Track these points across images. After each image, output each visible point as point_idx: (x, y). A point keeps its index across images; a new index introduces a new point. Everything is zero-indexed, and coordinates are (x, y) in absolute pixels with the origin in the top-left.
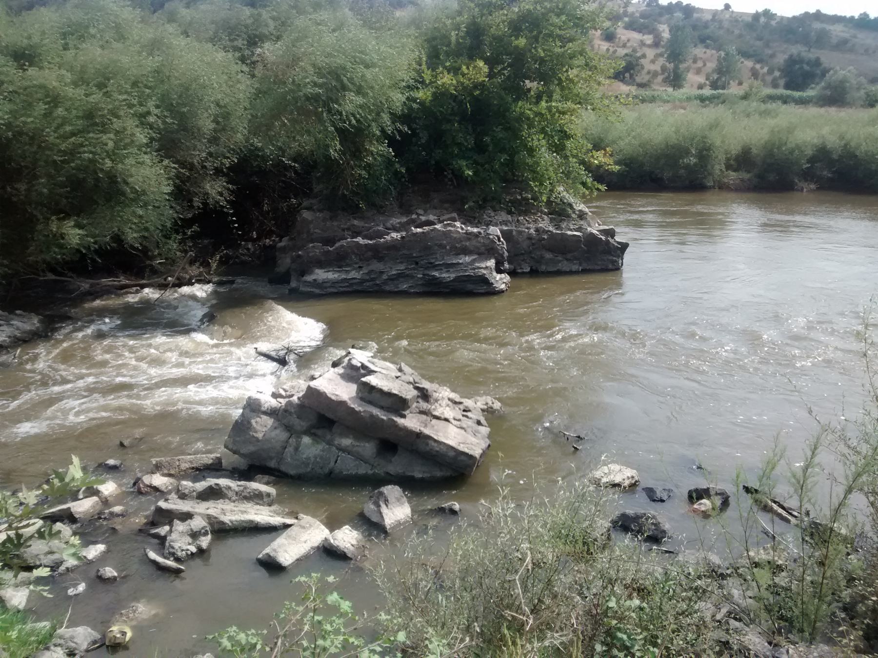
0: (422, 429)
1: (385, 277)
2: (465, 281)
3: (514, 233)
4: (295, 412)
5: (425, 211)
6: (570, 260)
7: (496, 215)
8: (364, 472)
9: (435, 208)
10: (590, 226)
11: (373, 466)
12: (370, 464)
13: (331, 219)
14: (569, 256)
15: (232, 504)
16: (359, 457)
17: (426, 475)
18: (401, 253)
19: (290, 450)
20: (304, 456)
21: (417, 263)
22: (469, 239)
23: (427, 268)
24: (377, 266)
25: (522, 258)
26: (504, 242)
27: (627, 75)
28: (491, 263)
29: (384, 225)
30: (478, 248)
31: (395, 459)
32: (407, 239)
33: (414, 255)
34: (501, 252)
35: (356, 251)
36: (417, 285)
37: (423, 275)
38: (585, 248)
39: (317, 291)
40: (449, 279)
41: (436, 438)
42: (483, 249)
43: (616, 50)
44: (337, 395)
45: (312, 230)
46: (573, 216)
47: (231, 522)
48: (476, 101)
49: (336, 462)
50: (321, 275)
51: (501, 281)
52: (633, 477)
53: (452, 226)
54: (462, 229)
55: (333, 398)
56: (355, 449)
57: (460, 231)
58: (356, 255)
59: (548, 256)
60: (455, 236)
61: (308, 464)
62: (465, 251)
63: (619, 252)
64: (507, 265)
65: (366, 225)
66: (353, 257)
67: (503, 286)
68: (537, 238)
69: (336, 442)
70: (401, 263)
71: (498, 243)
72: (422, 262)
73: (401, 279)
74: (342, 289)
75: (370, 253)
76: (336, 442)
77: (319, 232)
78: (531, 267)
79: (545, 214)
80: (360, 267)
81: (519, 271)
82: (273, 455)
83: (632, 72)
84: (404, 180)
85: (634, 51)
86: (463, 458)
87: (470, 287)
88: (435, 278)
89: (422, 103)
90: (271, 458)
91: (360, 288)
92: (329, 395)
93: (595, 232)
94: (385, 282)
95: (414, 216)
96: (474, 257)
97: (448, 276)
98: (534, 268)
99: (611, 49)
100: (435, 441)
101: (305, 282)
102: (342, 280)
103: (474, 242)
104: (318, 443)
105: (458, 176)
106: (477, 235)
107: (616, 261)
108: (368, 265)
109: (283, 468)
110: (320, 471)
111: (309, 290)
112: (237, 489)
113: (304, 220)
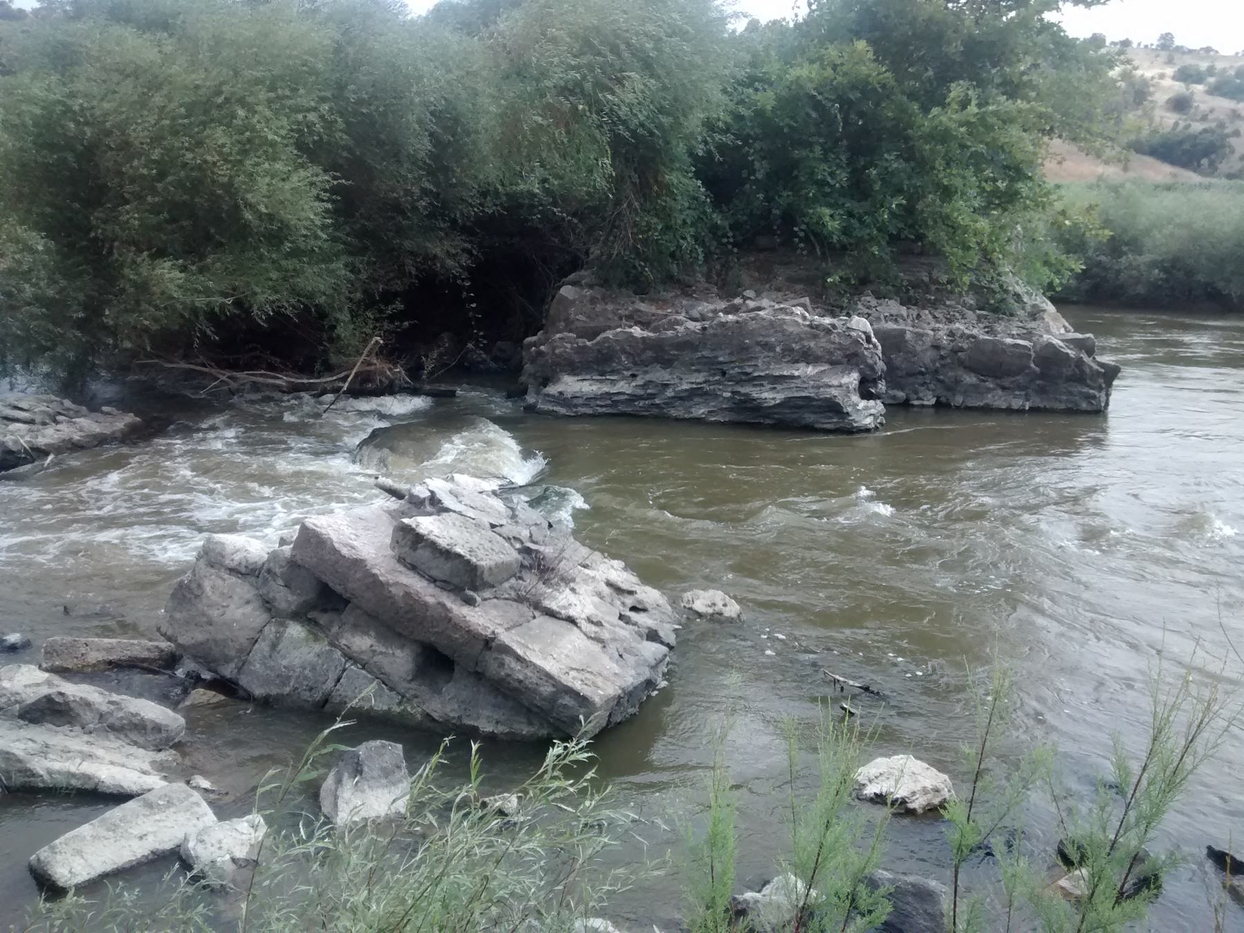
0: (499, 630)
1: (670, 393)
2: (801, 407)
3: (908, 336)
4: (282, 574)
5: (759, 294)
6: (1008, 388)
7: (881, 305)
8: (385, 708)
9: (779, 290)
10: (1048, 332)
11: (403, 697)
12: (398, 693)
13: (603, 299)
14: (1006, 382)
15: (86, 738)
16: (385, 681)
17: (501, 729)
18: (699, 354)
19: (263, 646)
20: (284, 662)
21: (724, 373)
22: (815, 337)
23: (738, 382)
24: (659, 375)
25: (920, 379)
26: (878, 344)
27: (1205, 162)
28: (853, 379)
29: (687, 313)
30: (831, 353)
31: (449, 689)
32: (711, 331)
33: (721, 359)
34: (870, 361)
35: (628, 348)
36: (722, 409)
37: (733, 392)
38: (1037, 369)
39: (563, 411)
40: (773, 403)
41: (520, 652)
42: (838, 355)
43: (1190, 125)
44: (353, 548)
45: (572, 316)
46: (1020, 313)
47: (50, 772)
48: (847, 105)
49: (338, 680)
50: (570, 385)
51: (867, 412)
52: (937, 790)
53: (787, 314)
54: (804, 318)
55: (345, 551)
56: (375, 659)
57: (800, 321)
58: (628, 354)
59: (970, 379)
60: (791, 329)
61: (289, 678)
62: (807, 357)
63: (1101, 381)
64: (882, 386)
65: (660, 312)
66: (623, 358)
67: (868, 421)
68: (950, 347)
69: (343, 642)
70: (698, 371)
71: (866, 345)
72: (731, 372)
73: (697, 399)
74: (600, 410)
75: (649, 353)
76: (343, 642)
77: (584, 319)
78: (938, 398)
79: (970, 308)
80: (634, 376)
81: (916, 403)
82: (233, 653)
83: (1213, 156)
84: (725, 240)
85: (1221, 125)
86: (567, 700)
87: (809, 418)
88: (748, 399)
89: (759, 113)
90: (227, 660)
91: (629, 409)
92: (336, 545)
93: (1056, 342)
94: (670, 403)
95: (738, 301)
96: (823, 368)
97: (769, 396)
98: (943, 399)
99: (1182, 124)
100: (519, 659)
101: (548, 395)
102: (602, 394)
103: (823, 342)
104: (316, 639)
105: (817, 236)
106: (828, 331)
107: (1094, 397)
108: (646, 372)
109: (244, 681)
110: (306, 695)
111: (551, 408)
112: (104, 708)
113: (564, 298)
